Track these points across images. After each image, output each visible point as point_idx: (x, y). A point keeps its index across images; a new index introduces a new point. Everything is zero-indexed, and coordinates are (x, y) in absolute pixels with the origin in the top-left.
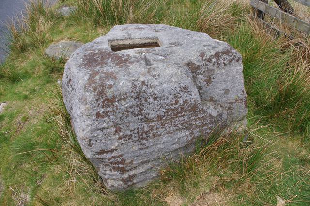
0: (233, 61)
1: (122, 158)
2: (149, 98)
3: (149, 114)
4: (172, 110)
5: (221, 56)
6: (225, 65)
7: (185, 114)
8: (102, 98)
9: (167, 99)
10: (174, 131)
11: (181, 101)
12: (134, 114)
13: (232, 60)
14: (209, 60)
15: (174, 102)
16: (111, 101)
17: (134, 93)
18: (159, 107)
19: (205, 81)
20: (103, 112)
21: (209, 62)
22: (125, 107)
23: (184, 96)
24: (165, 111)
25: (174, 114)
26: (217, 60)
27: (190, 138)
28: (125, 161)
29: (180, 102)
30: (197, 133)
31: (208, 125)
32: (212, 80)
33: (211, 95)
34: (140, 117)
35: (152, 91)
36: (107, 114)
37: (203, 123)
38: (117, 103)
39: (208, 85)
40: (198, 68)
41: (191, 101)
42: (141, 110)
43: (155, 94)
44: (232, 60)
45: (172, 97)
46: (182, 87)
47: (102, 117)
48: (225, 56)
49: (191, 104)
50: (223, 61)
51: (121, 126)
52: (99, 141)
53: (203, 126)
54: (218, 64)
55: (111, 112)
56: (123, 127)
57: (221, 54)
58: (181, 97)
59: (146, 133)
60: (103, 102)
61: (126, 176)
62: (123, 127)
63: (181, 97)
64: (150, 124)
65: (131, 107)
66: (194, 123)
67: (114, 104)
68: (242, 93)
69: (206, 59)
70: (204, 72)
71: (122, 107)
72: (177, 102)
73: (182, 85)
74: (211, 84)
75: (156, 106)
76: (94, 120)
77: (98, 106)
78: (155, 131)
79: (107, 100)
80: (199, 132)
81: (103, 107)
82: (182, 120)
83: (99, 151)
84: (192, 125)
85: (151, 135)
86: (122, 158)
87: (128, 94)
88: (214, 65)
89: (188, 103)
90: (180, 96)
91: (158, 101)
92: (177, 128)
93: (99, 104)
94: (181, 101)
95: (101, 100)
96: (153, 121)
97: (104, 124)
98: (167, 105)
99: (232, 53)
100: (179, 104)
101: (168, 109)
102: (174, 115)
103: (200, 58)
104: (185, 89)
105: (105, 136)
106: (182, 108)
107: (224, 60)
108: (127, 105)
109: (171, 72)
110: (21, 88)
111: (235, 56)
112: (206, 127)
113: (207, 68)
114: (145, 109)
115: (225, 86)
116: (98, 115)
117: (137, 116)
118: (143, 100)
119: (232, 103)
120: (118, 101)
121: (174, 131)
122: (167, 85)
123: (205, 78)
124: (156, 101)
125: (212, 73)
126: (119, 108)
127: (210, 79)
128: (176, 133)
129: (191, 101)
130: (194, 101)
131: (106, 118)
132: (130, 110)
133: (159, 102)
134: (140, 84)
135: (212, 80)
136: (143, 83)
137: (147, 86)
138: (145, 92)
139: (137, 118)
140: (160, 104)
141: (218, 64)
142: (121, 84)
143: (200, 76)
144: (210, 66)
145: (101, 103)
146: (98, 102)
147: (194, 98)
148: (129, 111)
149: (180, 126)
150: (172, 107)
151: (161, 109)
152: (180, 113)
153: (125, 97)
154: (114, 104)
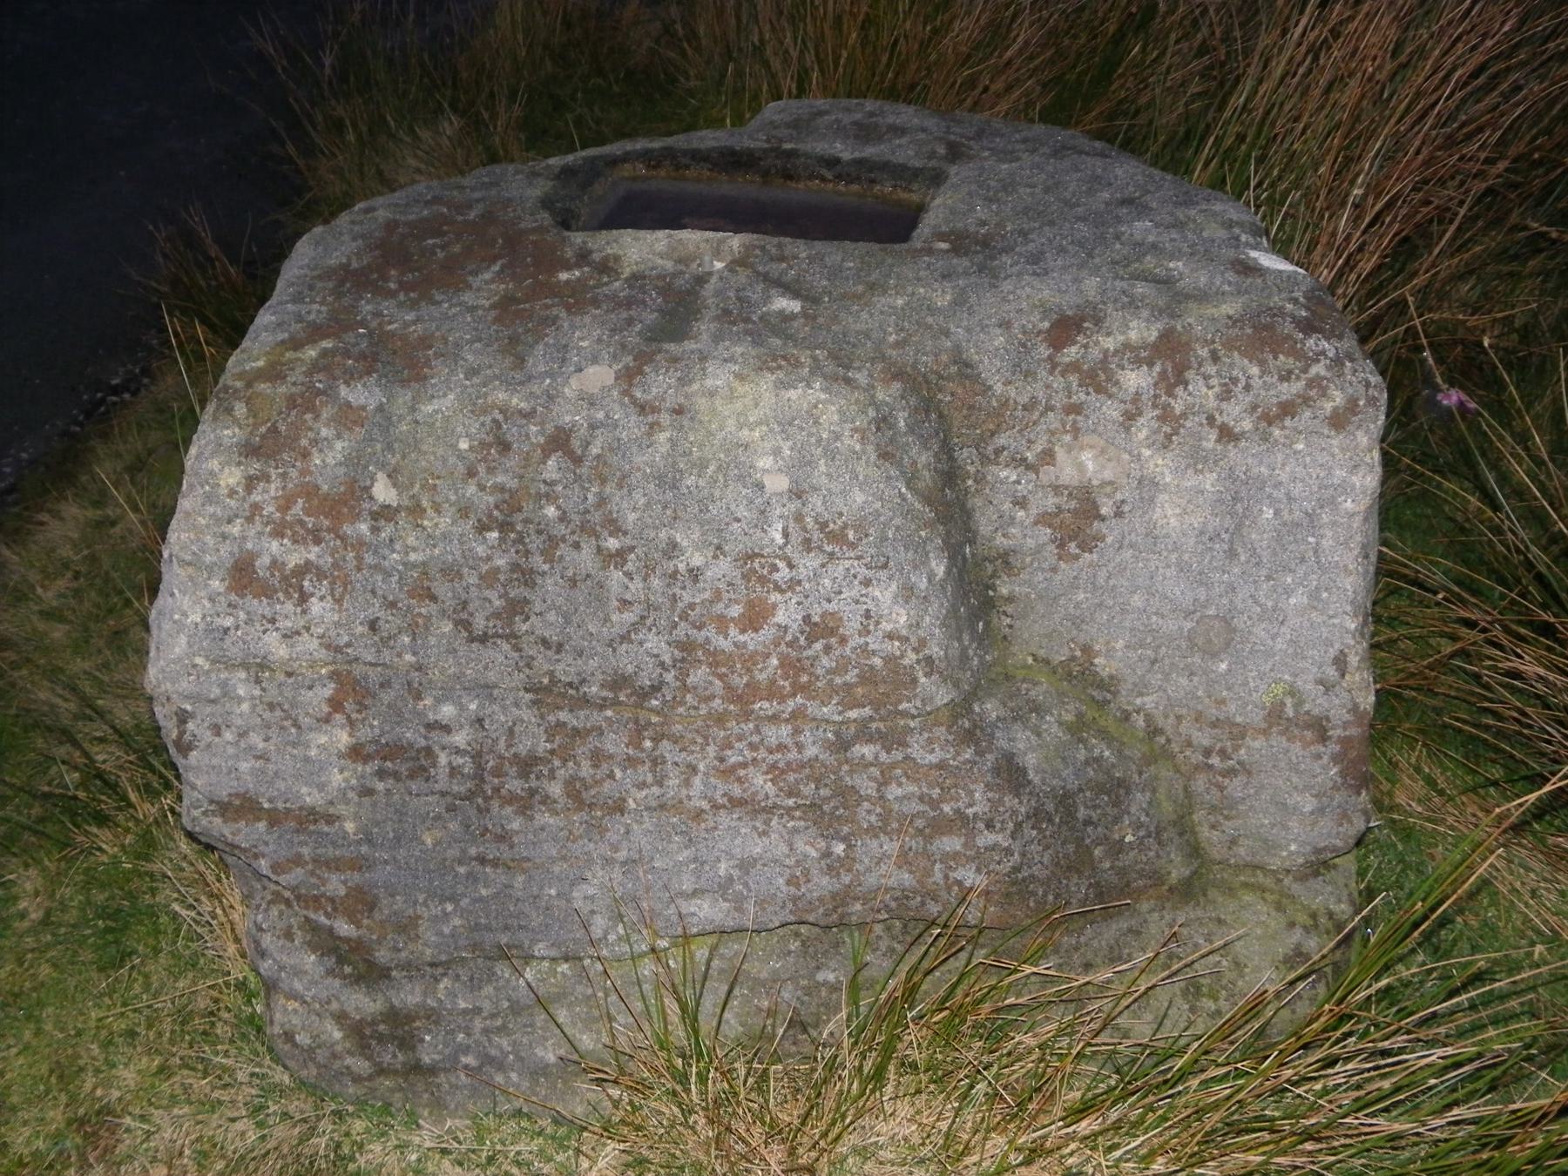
1: (356, 878)
2: (577, 546)
6: (1227, 434)
7: (813, 708)
8: (284, 476)
10: (716, 807)
11: (787, 614)
13: (1288, 409)
15: (736, 611)
19: (1044, 519)
25: (728, 688)
27: (823, 884)
28: (372, 906)
29: (780, 617)
30: (882, 866)
31: (971, 835)
36: (294, 584)
37: (934, 804)
47: (266, 592)
49: (864, 650)
52: (228, 736)
53: (939, 826)
54: (1166, 416)
55: (321, 574)
59: (527, 765)
61: (362, 1003)
64: (563, 716)
66: (868, 787)
67: (347, 529)
68: (1332, 672)
69: (1074, 367)
72: (755, 617)
74: (1085, 547)
78: (586, 770)
80: (904, 859)
81: (278, 534)
82: (781, 747)
83: (223, 794)
84: (847, 795)
85: (555, 789)
86: (356, 878)
88: (1130, 417)
89: (843, 640)
90: (784, 573)
92: (737, 791)
94: (787, 614)
96: (585, 701)
98: (684, 616)
100: (767, 633)
102: (732, 695)
105: (267, 715)
106: (791, 666)
110: (1556, 1108)
112: (951, 843)
114: (538, 607)
119: (1240, 733)
121: (716, 807)
123: (1051, 502)
128: (724, 819)
145: (269, 509)
149: (760, 782)
152: (773, 692)
154: (347, 529)
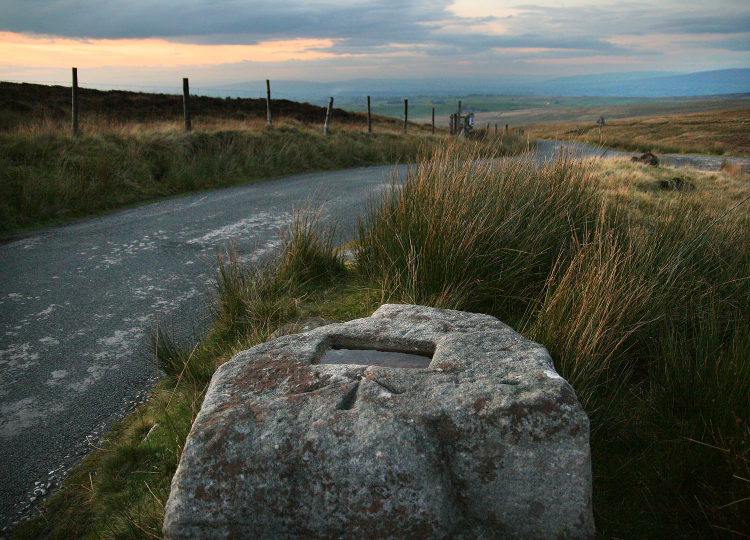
0: (562, 433)
3: (308, 518)
4: (363, 523)
5: (525, 415)
6: (537, 439)
8: (216, 458)
9: (355, 492)
11: (387, 506)
12: (276, 511)
13: (557, 429)
14: (492, 420)
15: (369, 505)
16: (233, 468)
17: (283, 462)
18: (333, 508)
20: (211, 488)
21: (492, 424)
22: (256, 489)
23: (400, 496)
24: (344, 519)
26: (514, 422)
32: (496, 472)
33: (493, 509)
34: (289, 520)
35: (323, 468)
36: (216, 495)
38: (242, 476)
39: (483, 482)
40: (459, 434)
41: (413, 512)
42: (293, 504)
43: (328, 476)
44: (557, 429)
45: (364, 491)
46: (395, 475)
48: (541, 417)
50: (530, 428)
51: (244, 529)
54: (515, 433)
56: (247, 532)
57: (526, 410)
58: (388, 496)
60: (215, 467)
62: (247, 532)
63: (388, 496)
65: (271, 492)
68: (579, 522)
69: (484, 417)
70: (476, 447)
71: (252, 488)
72: (376, 507)
73: (396, 467)
75: (326, 503)
76: (190, 501)
77: (204, 473)
79: (225, 464)
87: (269, 463)
91: (332, 493)
93: (206, 469)
94: (387, 506)
95: (213, 462)
97: (207, 515)
99: (558, 411)
100: (380, 513)
101: (353, 518)
103: (472, 411)
104: (402, 480)
107: (535, 425)
108: (261, 486)
109: (379, 432)
111: (565, 420)
113: (485, 438)
114: (301, 504)
115: (531, 494)
116: (200, 493)
117: (282, 515)
118: (300, 482)
120: (246, 472)
122: (361, 460)
123: (478, 463)
124: (328, 493)
125: (497, 453)
126: (243, 487)
127: (491, 465)
129: (413, 512)
130: (423, 514)
131: (215, 504)
132: (268, 498)
133: (335, 496)
134: (301, 447)
135: (496, 472)
136: (309, 444)
137: (315, 453)
138: (306, 466)
139: (280, 519)
140: (337, 501)
141: (515, 433)
142: (262, 437)
143: (463, 454)
144: (493, 434)
145: (210, 469)
146: (206, 465)
147: (423, 507)
148: (265, 501)
150: (363, 516)
151: (336, 514)
153: (263, 466)
